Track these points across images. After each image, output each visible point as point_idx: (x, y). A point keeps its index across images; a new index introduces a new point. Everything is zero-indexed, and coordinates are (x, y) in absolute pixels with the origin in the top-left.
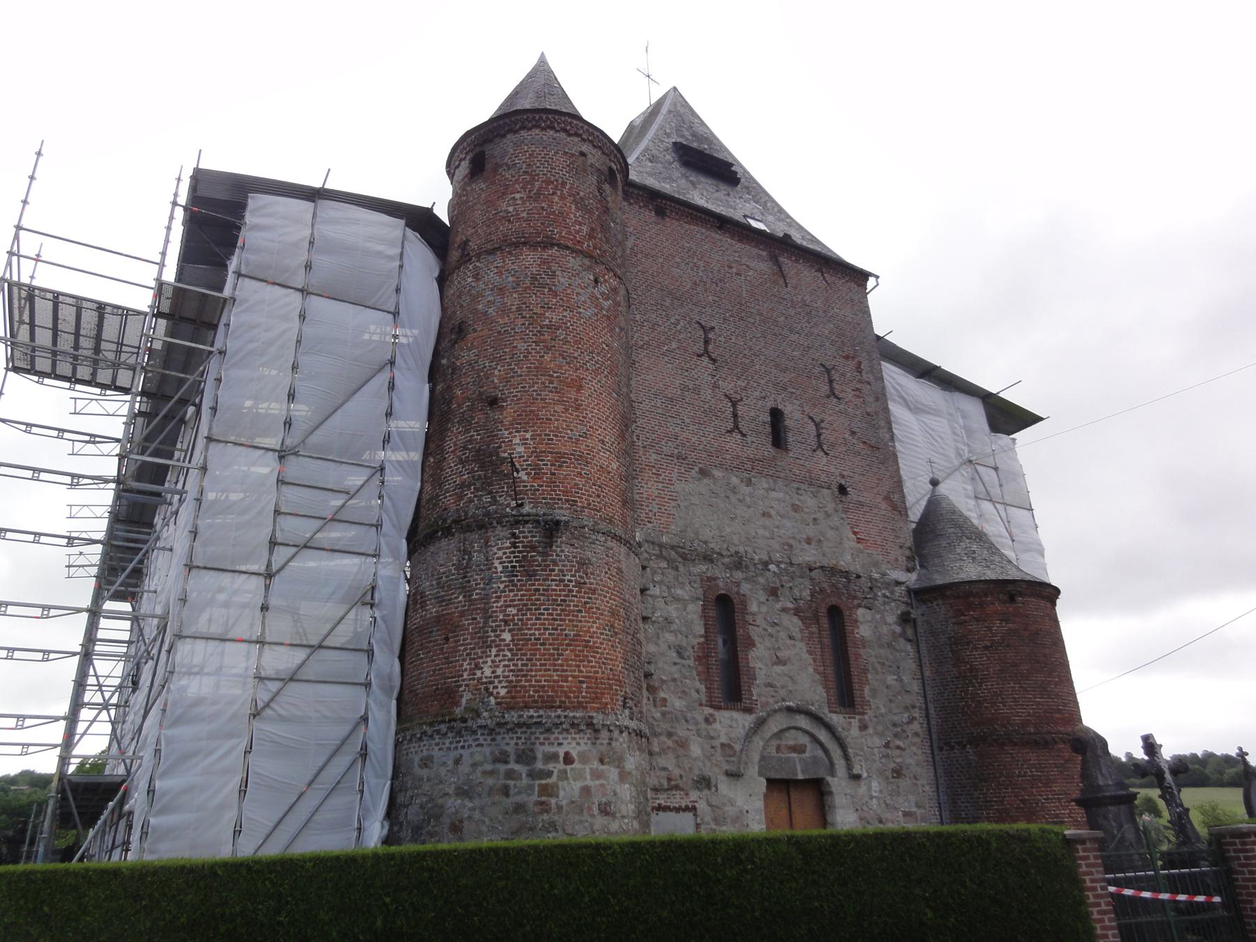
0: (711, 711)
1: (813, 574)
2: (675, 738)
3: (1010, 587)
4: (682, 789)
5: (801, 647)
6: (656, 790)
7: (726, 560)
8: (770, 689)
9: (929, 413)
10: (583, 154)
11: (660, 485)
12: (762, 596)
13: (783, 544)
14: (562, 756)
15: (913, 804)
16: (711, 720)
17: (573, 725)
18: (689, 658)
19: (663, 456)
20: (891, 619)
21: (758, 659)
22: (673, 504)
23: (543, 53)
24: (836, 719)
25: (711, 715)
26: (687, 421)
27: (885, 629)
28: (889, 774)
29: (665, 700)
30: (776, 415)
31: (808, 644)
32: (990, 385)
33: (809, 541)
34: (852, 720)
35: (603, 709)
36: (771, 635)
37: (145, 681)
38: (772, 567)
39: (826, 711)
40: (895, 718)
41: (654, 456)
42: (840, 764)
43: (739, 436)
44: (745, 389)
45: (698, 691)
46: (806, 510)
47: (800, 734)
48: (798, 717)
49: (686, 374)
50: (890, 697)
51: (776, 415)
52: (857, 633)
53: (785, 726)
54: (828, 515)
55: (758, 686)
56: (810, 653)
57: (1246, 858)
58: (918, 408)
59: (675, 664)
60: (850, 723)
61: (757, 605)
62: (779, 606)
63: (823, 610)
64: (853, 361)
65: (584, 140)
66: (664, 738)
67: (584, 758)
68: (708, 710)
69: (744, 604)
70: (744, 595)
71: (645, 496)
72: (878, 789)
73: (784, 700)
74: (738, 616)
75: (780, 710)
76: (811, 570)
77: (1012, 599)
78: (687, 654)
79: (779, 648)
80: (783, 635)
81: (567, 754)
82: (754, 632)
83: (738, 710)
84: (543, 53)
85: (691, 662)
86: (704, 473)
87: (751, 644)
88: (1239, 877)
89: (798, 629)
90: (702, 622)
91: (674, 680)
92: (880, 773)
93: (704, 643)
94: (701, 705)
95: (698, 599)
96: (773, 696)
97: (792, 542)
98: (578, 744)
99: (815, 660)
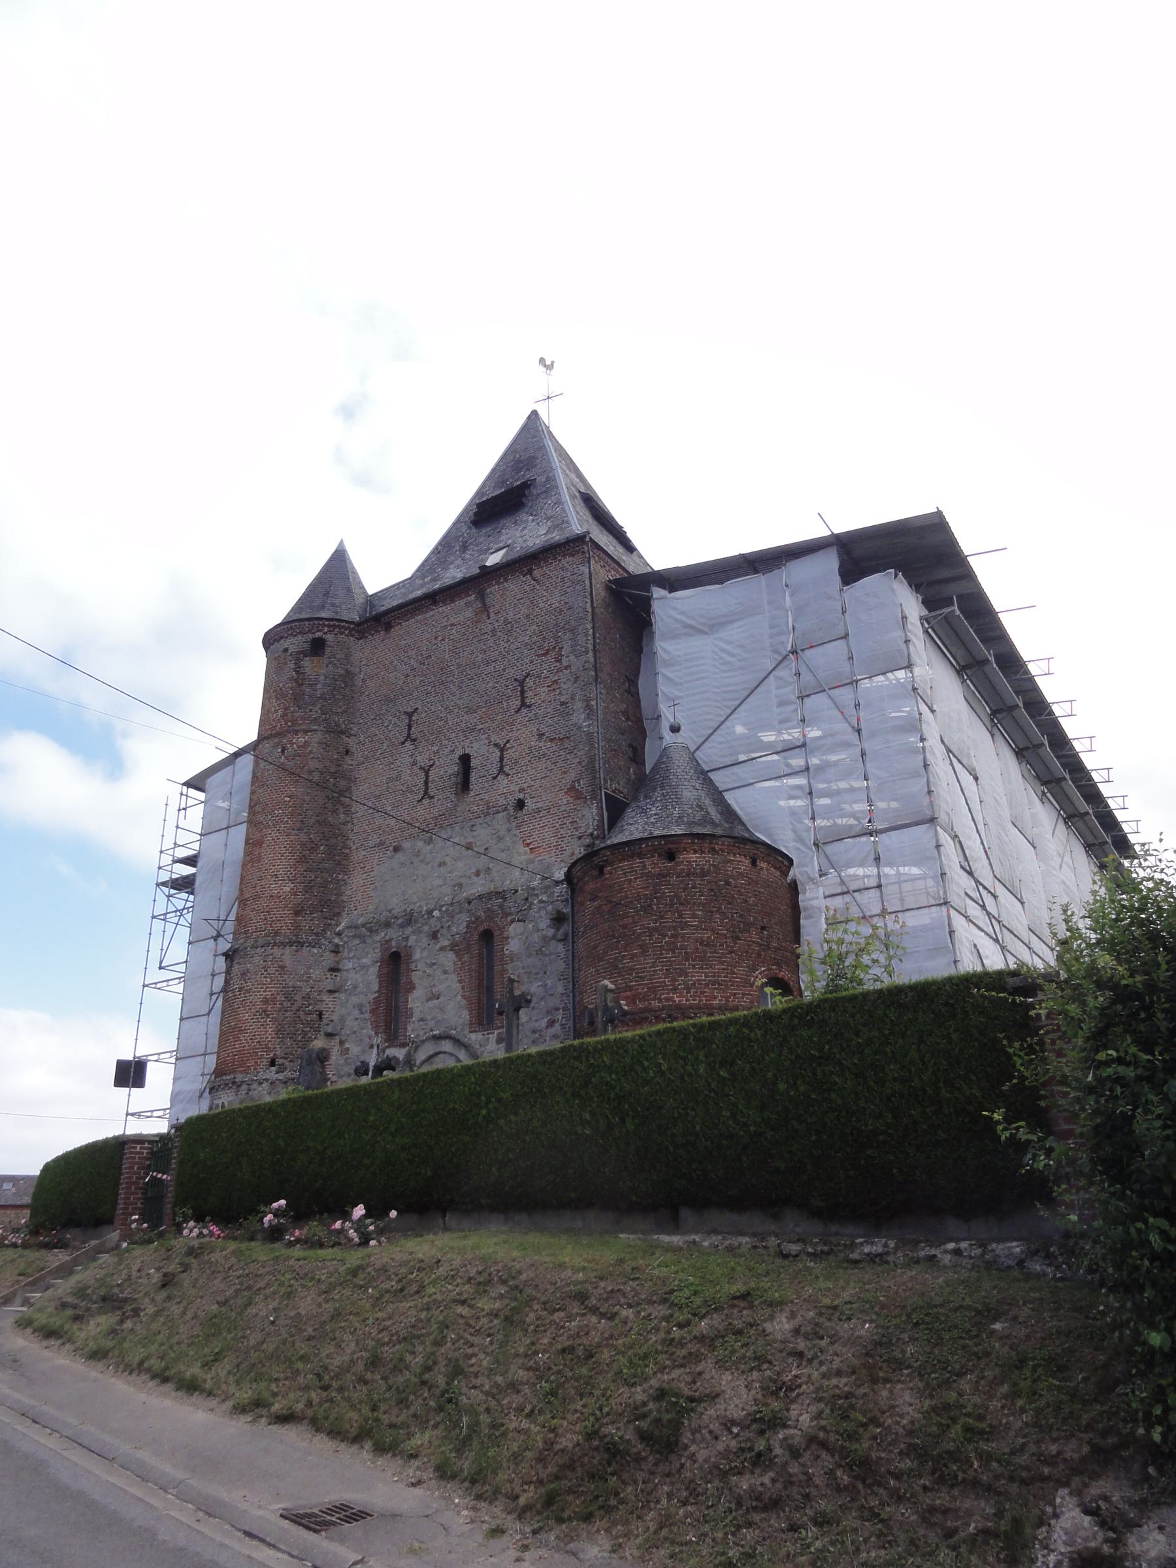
1: (472, 906)
5: (453, 978)
7: (400, 921)
9: (732, 622)
10: (286, 650)
12: (425, 941)
13: (454, 886)
17: (227, 1084)
20: (544, 923)
21: (416, 1001)
23: (342, 541)
27: (536, 937)
30: (465, 760)
32: (818, 531)
33: (477, 874)
34: (491, 1036)
35: (246, 1072)
36: (429, 975)
37: (1042, 950)
38: (436, 913)
39: (466, 1031)
40: (536, 1025)
46: (478, 844)
47: (446, 1056)
48: (443, 1042)
51: (465, 760)
53: (431, 1053)
54: (500, 839)
55: (413, 1022)
56: (460, 982)
58: (714, 625)
59: (357, 1019)
61: (421, 953)
65: (286, 638)
73: (432, 1030)
74: (403, 967)
75: (427, 1039)
76: (469, 903)
77: (671, 856)
78: (364, 1009)
80: (438, 972)
82: (415, 977)
83: (395, 1046)
84: (342, 541)
85: (367, 1015)
86: (397, 849)
87: (411, 987)
88: (140, 1196)
91: (354, 1032)
93: (378, 997)
95: (377, 962)
97: (462, 880)
99: (463, 988)
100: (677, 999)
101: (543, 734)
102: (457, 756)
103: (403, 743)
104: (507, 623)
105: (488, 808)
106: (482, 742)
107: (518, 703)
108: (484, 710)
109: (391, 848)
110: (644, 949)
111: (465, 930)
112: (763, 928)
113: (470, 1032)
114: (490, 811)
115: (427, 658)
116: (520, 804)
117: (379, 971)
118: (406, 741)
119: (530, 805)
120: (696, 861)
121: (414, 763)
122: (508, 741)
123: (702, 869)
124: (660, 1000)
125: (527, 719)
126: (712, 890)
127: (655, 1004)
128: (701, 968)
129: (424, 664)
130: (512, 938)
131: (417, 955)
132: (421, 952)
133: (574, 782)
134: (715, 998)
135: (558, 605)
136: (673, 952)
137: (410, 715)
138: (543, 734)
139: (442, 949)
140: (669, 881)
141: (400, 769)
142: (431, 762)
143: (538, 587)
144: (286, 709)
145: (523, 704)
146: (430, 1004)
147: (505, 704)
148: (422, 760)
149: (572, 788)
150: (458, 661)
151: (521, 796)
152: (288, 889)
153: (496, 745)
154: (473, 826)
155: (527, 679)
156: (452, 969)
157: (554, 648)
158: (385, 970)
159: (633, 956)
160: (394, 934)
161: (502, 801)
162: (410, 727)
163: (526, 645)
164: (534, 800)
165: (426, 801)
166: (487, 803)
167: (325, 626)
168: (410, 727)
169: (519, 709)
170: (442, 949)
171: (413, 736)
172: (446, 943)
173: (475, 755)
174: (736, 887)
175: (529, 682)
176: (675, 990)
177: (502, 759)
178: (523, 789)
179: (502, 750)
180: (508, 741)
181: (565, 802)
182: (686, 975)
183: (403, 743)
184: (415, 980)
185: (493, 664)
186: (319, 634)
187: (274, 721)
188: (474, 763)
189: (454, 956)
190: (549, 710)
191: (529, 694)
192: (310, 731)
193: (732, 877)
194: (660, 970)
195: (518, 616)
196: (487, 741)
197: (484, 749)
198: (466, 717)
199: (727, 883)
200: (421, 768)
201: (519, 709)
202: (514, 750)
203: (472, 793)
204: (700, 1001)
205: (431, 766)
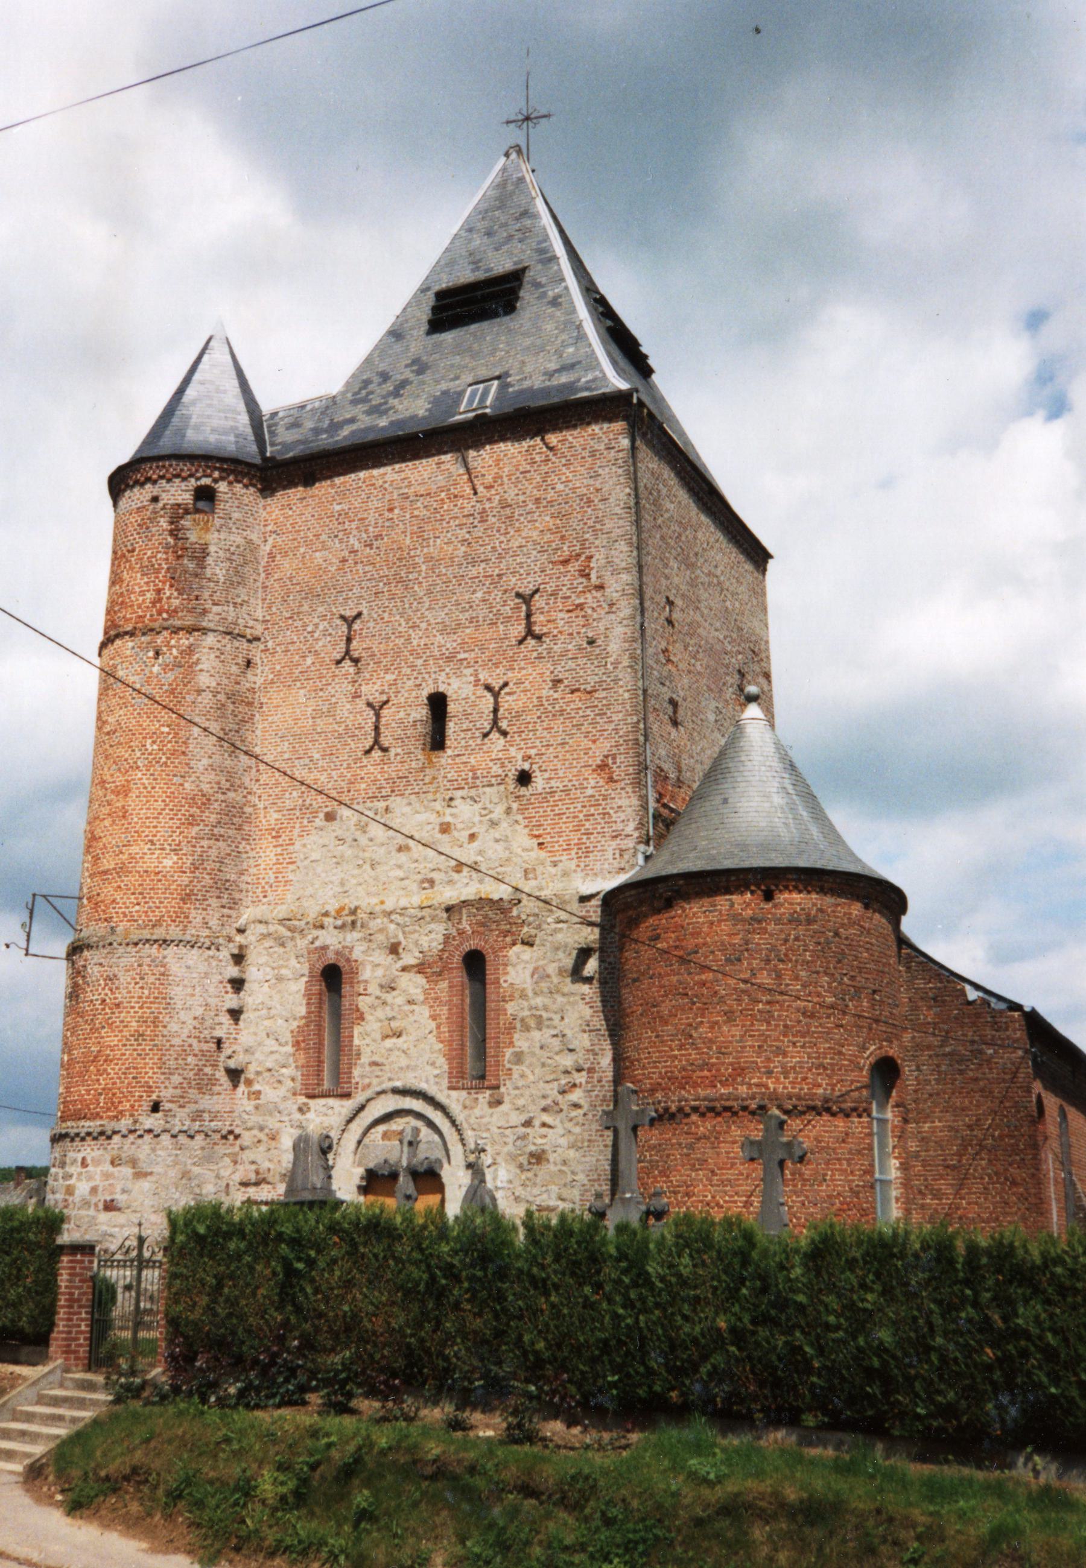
0: (305, 1100)
2: (267, 1131)
3: (661, 888)
4: (269, 1183)
6: (245, 1184)
8: (374, 1068)
11: (279, 850)
14: (80, 1160)
15: (554, 1196)
16: (305, 1109)
18: (287, 1043)
19: (285, 812)
22: (292, 867)
24: (454, 1100)
25: (305, 1104)
26: (316, 756)
28: (523, 1160)
29: (259, 1092)
30: (438, 703)
31: (431, 1007)
34: (480, 1096)
41: (276, 816)
42: (456, 1150)
43: (380, 753)
44: (395, 683)
45: (293, 1080)
46: (459, 826)
49: (321, 694)
50: (542, 1060)
51: (438, 703)
52: (505, 981)
56: (434, 1017)
57: (74, 1268)
60: (477, 1099)
62: (400, 964)
63: (457, 960)
64: (577, 560)
66: (255, 1132)
67: (97, 1162)
68: (302, 1099)
69: (354, 972)
70: (356, 961)
71: (262, 867)
72: (505, 1179)
79: (394, 1018)
81: (84, 1159)
86: (330, 817)
89: (419, 991)
90: (304, 1002)
92: (512, 1157)
94: (295, 1094)
96: (377, 1077)
97: (434, 875)
98: (92, 1150)
100: (771, 1086)
101: (560, 681)
102: (425, 693)
103: (339, 662)
104: (505, 505)
105: (475, 778)
106: (464, 679)
107: (520, 629)
108: (468, 631)
109: (321, 815)
110: (729, 1015)
111: (441, 947)
112: (874, 992)
113: (451, 1088)
114: (474, 780)
115: (376, 538)
116: (524, 778)
117: (306, 989)
118: (343, 659)
119: (539, 782)
120: (800, 904)
121: (356, 696)
122: (506, 684)
123: (808, 915)
124: (750, 1085)
125: (535, 654)
126: (819, 943)
127: (743, 1090)
128: (803, 1047)
129: (371, 546)
130: (514, 966)
131: (366, 974)
132: (373, 971)
133: (606, 757)
134: (820, 1086)
135: (585, 491)
136: (769, 1023)
137: (349, 621)
138: (560, 681)
139: (404, 969)
140: (766, 929)
141: (334, 700)
142: (384, 698)
143: (554, 459)
144: (159, 591)
145: (530, 633)
146: (389, 1043)
147: (501, 627)
148: (371, 691)
149: (603, 767)
150: (425, 550)
151: (526, 766)
152: (170, 863)
153: (488, 688)
154: (451, 799)
155: (537, 597)
156: (421, 998)
157: (579, 555)
158: (316, 989)
159: (714, 1025)
160: (330, 938)
161: (496, 769)
162: (349, 640)
163: (535, 543)
164: (546, 775)
165: (377, 754)
166: (473, 770)
167: (216, 468)
168: (349, 640)
169: (524, 639)
170: (404, 969)
171: (356, 655)
172: (413, 962)
173: (454, 697)
174: (847, 939)
175: (539, 602)
176: (769, 1073)
177: (496, 711)
178: (530, 757)
179: (496, 695)
180: (506, 684)
181: (592, 782)
182: (785, 1054)
183: (339, 662)
184: (363, 1003)
185: (483, 565)
186: (206, 481)
187: (139, 607)
188: (452, 708)
189: (424, 981)
190: (570, 647)
191: (538, 618)
192: (198, 630)
193: (843, 925)
194: (750, 1047)
195: (521, 498)
196: (472, 679)
197: (468, 690)
198: (439, 638)
199: (837, 934)
200: (369, 705)
201: (524, 639)
202: (515, 697)
203: (449, 752)
204: (802, 1089)
205: (386, 702)
